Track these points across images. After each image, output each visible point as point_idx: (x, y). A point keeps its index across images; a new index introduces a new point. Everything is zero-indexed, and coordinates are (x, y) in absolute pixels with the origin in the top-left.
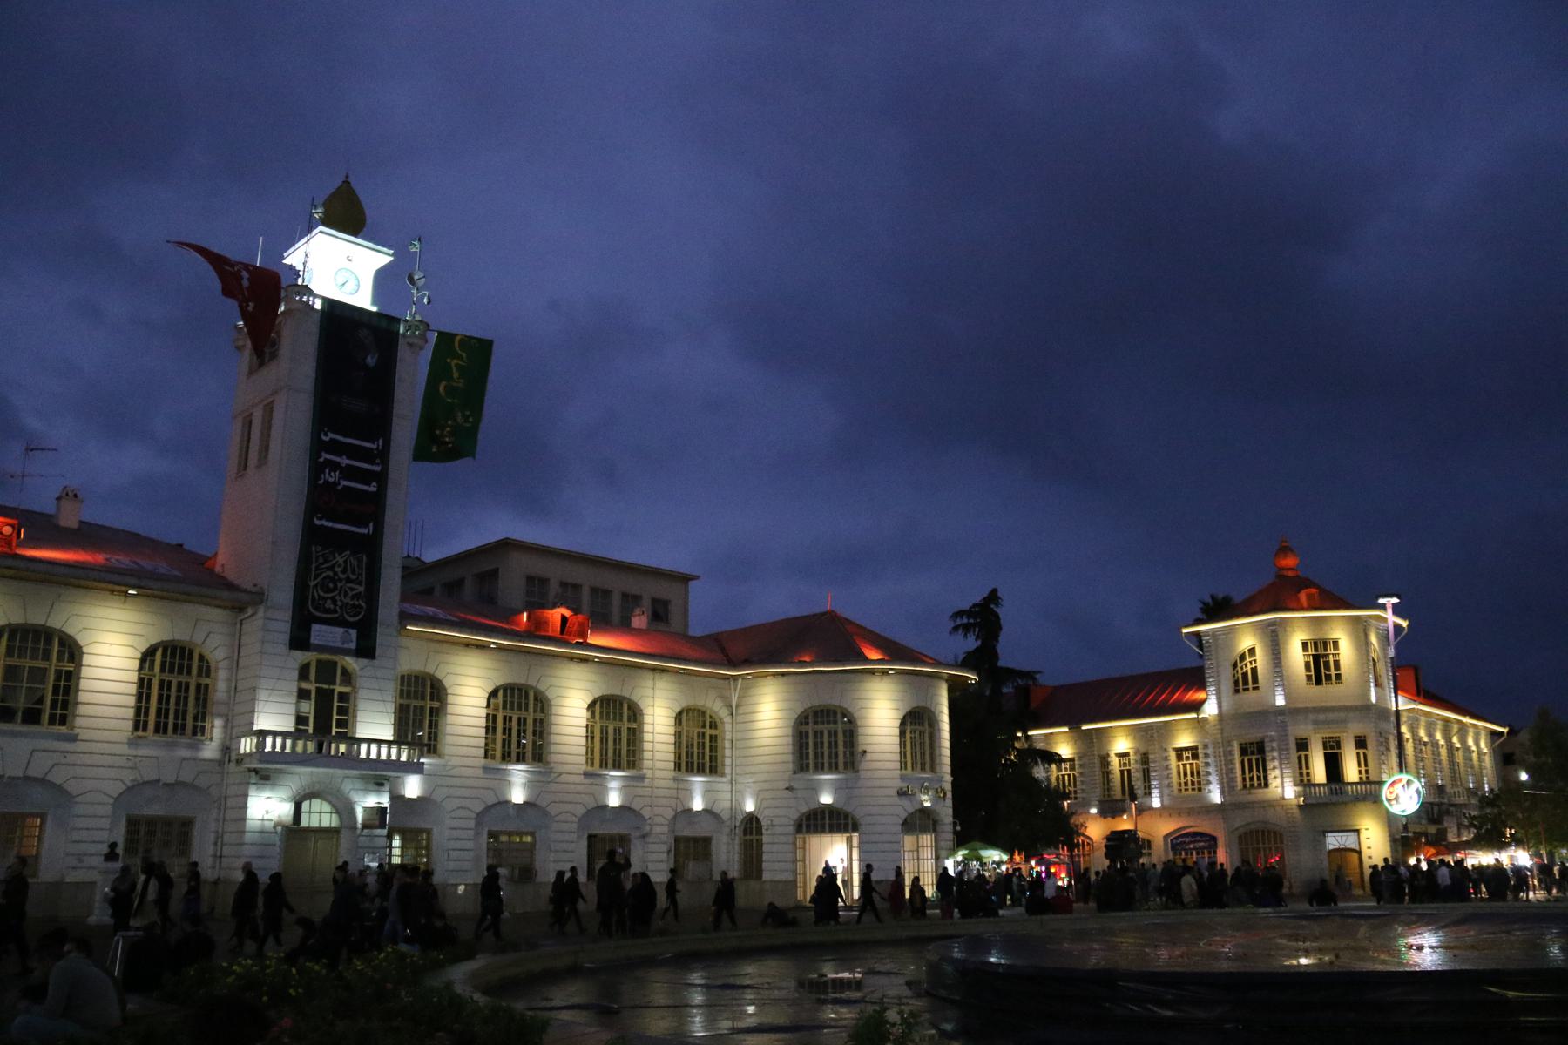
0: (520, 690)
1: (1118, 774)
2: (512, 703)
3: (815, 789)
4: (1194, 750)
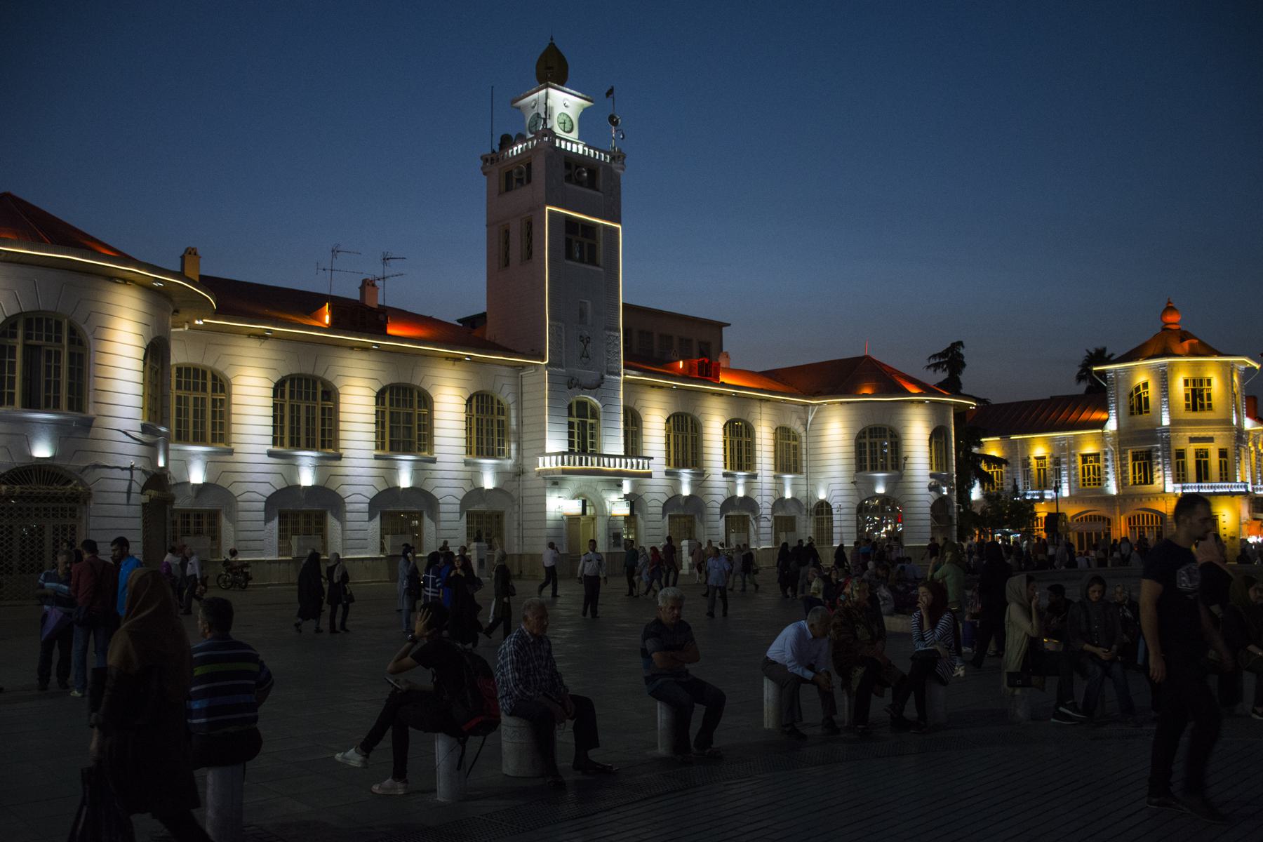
0: (307, 380)
3: (872, 483)
4: (1096, 456)
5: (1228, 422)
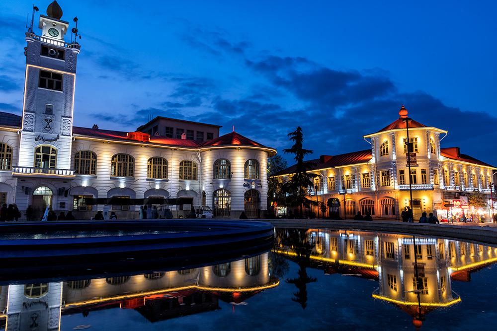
0: (124, 155)
1: (346, 182)
2: (156, 162)
5: (426, 157)
